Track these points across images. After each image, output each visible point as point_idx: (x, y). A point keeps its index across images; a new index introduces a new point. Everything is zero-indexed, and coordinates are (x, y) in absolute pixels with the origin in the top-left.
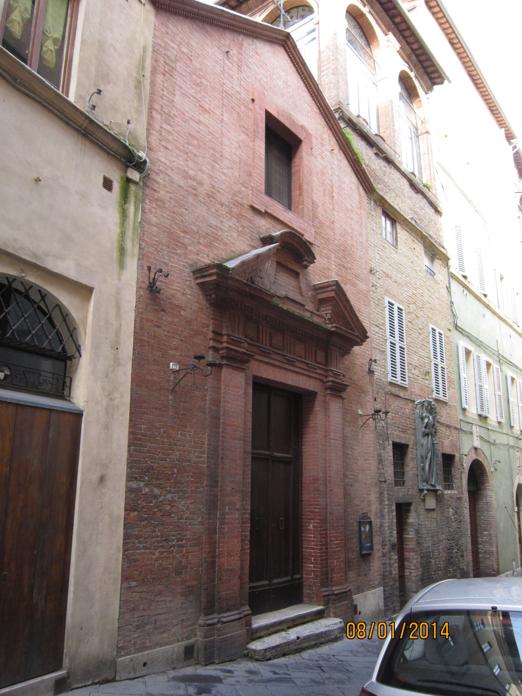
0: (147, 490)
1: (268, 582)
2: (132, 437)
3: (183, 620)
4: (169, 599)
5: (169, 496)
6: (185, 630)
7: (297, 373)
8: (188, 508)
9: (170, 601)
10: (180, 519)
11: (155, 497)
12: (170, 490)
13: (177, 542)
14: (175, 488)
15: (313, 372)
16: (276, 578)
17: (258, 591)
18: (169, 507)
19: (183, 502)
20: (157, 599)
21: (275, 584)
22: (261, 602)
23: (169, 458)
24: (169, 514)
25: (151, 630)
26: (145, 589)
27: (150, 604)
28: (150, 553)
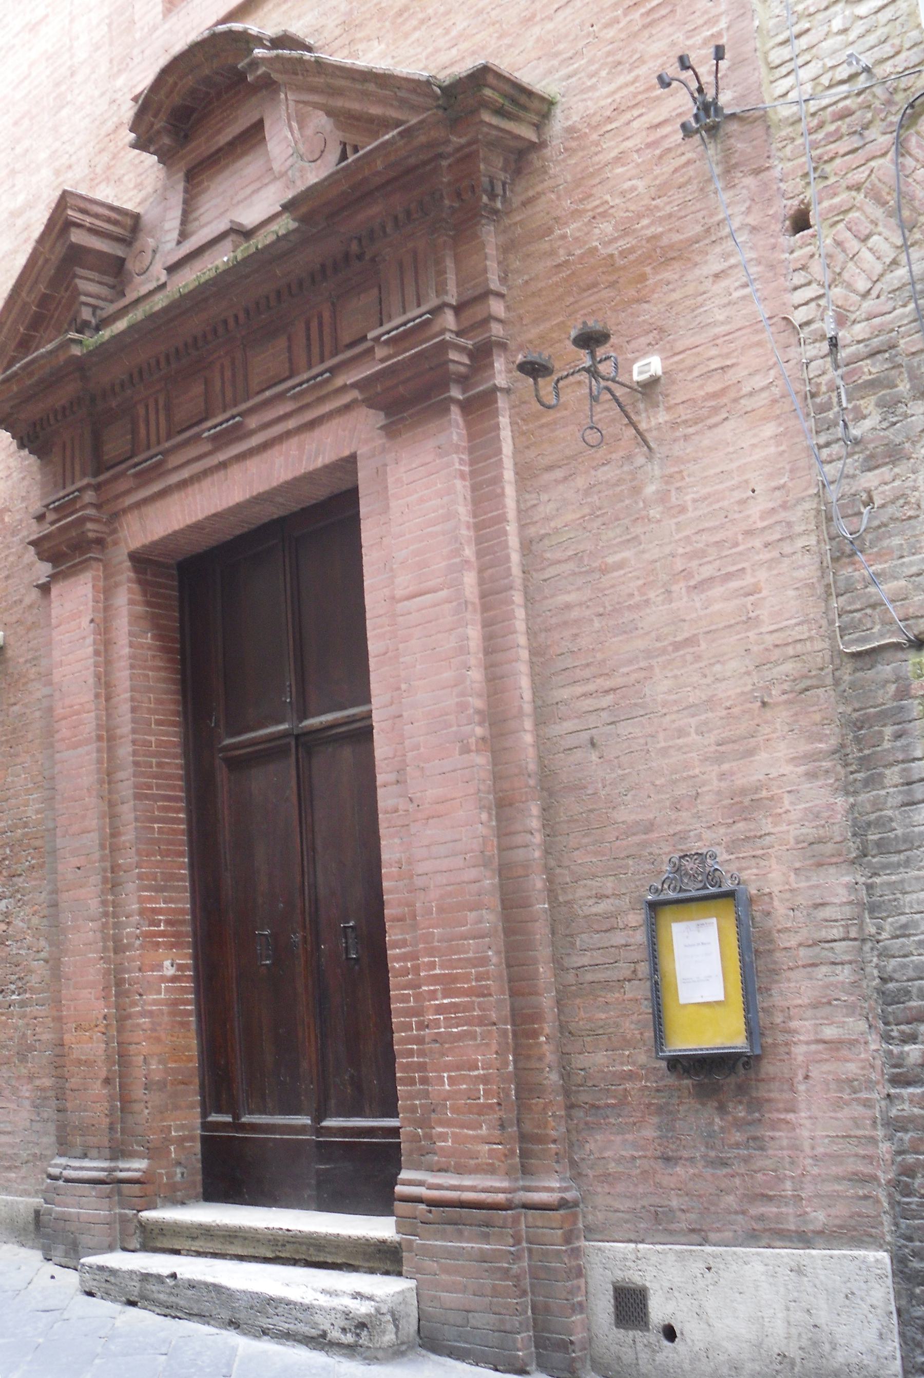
7: (265, 446)
15: (321, 400)
21: (330, 1131)
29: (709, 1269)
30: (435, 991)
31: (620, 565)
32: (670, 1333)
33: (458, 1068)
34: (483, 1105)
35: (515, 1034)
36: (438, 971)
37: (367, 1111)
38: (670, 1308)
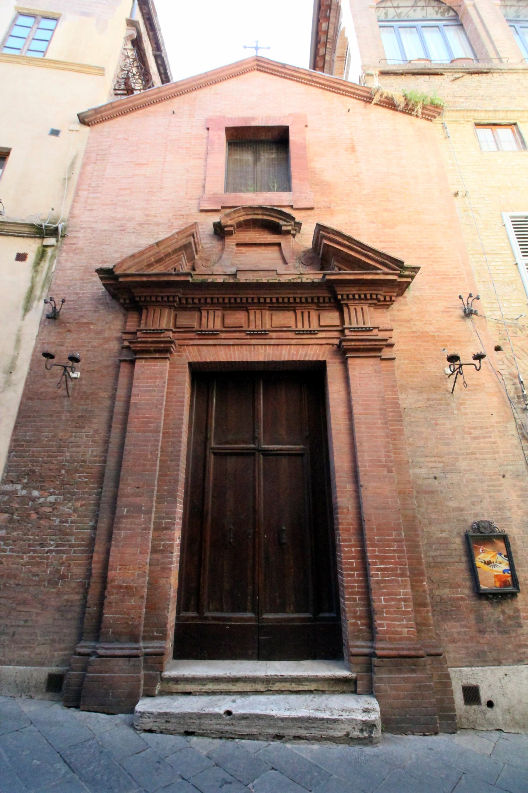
0: (24, 492)
1: (311, 616)
2: (13, 444)
3: (53, 641)
4: (35, 610)
5: (52, 499)
6: (56, 654)
8: (75, 511)
9: (37, 614)
10: (63, 522)
11: (34, 499)
12: (54, 492)
13: (57, 547)
14: (61, 489)
16: (270, 612)
17: (229, 625)
18: (50, 510)
19: (70, 504)
20: (19, 608)
22: (194, 643)
23: (57, 460)
24: (48, 517)
25: (7, 643)
26: (5, 595)
27: (9, 612)
28: (17, 556)
29: (506, 675)
30: (376, 562)
31: (444, 424)
32: (490, 704)
33: (389, 594)
34: (404, 611)
35: (411, 580)
36: (377, 554)
37: (288, 609)
38: (489, 693)
